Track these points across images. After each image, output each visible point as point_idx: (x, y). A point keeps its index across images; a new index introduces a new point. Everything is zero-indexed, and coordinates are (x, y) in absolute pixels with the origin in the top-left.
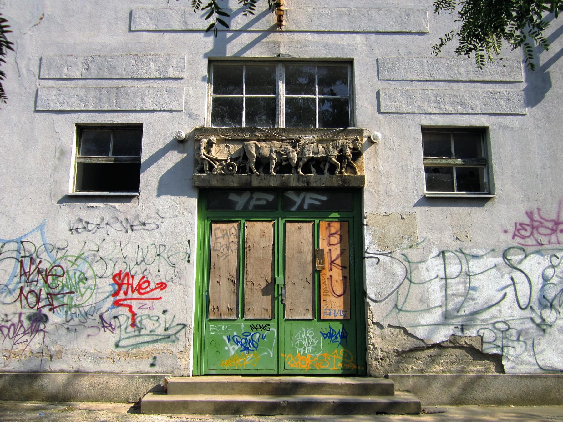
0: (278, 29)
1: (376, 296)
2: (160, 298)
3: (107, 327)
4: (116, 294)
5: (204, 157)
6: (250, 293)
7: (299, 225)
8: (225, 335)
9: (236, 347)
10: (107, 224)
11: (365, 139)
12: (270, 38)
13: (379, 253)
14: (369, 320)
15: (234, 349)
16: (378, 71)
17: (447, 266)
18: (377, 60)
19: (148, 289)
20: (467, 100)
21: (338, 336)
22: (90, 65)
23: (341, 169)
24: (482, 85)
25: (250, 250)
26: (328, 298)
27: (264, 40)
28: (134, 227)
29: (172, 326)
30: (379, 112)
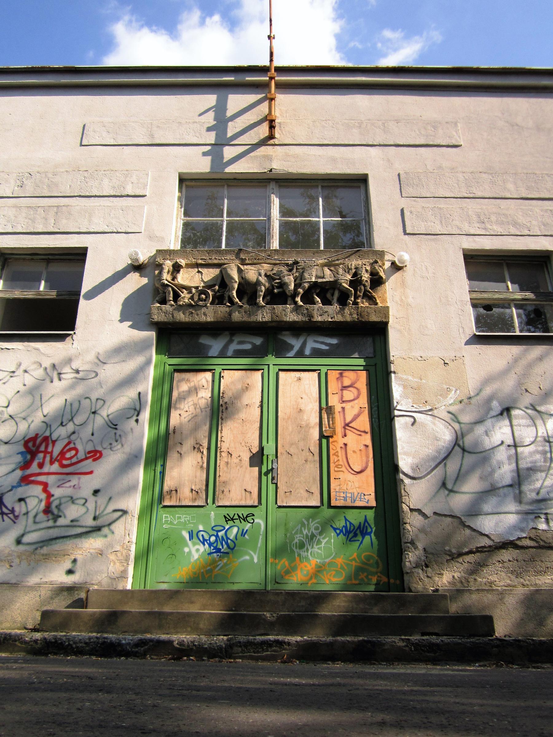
0: (272, 142)
1: (413, 470)
2: (91, 472)
3: (7, 514)
4: (26, 465)
5: (166, 282)
6: (225, 469)
7: (297, 374)
8: (185, 529)
9: (202, 548)
10: (26, 371)
11: (387, 265)
12: (260, 152)
13: (414, 410)
14: (404, 506)
15: (198, 550)
16: (400, 187)
17: (515, 428)
18: (399, 175)
19: (74, 460)
20: (521, 220)
21: (358, 532)
22: (25, 182)
23: (356, 297)
24: (540, 202)
25: (227, 408)
26: (341, 475)
27: (252, 154)
28: (63, 376)
29: (105, 512)
30: (405, 233)
